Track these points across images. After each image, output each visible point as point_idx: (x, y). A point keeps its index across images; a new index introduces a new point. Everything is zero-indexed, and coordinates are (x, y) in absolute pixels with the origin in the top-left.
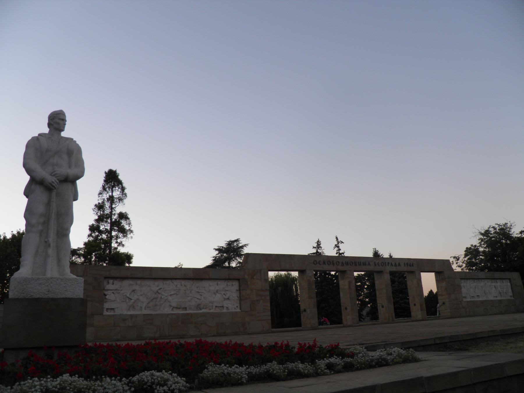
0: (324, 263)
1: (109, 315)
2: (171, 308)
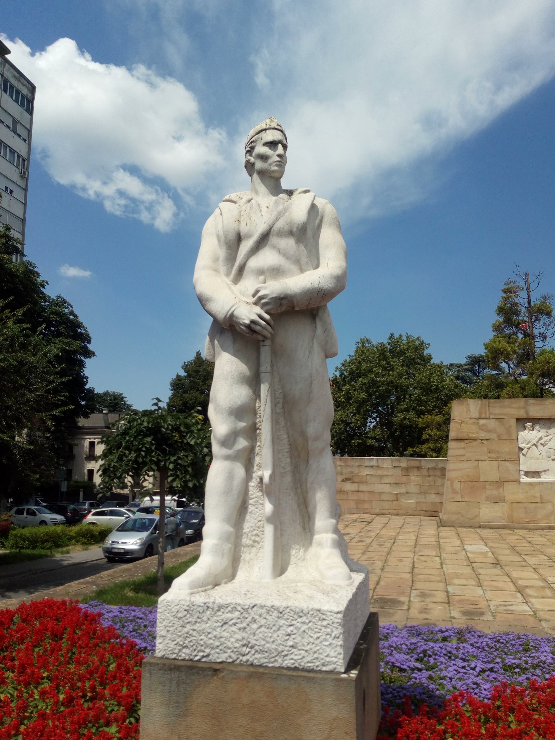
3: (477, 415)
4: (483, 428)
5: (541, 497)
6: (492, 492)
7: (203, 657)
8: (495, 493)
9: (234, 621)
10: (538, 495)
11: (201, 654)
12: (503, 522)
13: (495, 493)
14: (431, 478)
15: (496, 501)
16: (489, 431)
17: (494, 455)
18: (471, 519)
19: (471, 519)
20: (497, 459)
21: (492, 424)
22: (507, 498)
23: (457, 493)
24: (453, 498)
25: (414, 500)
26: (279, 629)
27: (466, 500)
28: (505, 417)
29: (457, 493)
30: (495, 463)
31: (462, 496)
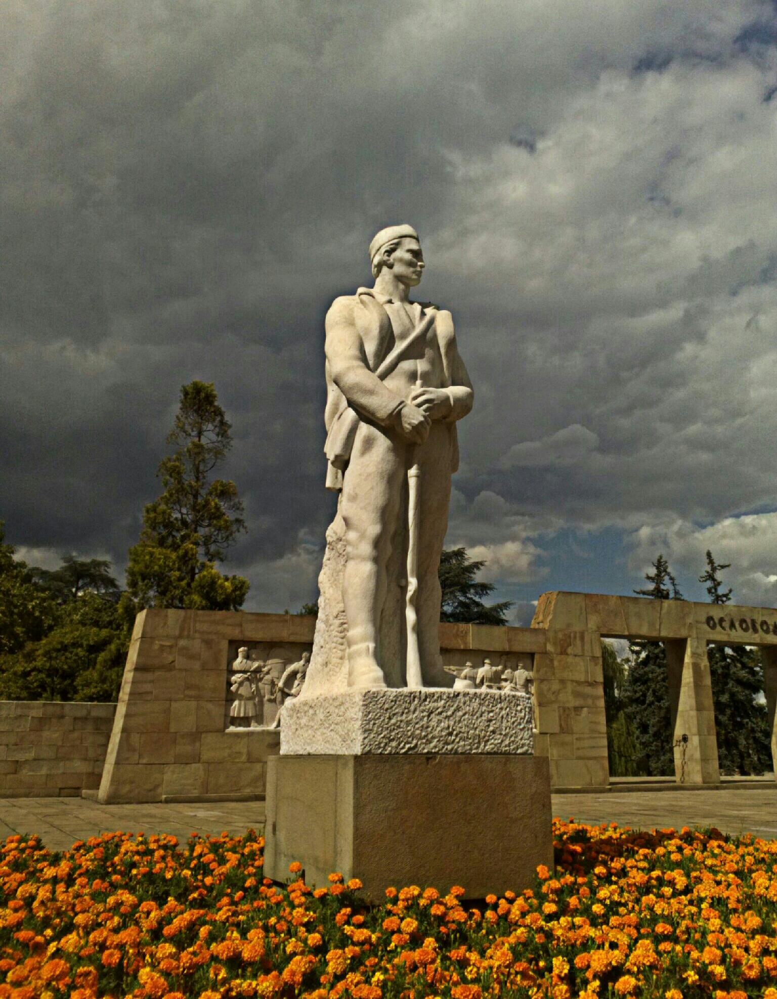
0: (732, 625)
1: (237, 735)
2: (397, 329)
3: (177, 633)
4: (184, 651)
5: (249, 754)
6: (184, 748)
7: (410, 749)
8: (189, 748)
9: (440, 710)
10: (245, 751)
11: (407, 746)
12: (195, 793)
13: (189, 748)
14: (76, 734)
15: (184, 761)
16: (192, 657)
17: (193, 693)
18: (150, 791)
19: (150, 791)
20: (198, 698)
21: (196, 645)
22: (205, 757)
23: (134, 750)
24: (127, 759)
25: (44, 771)
26: (481, 716)
27: (144, 761)
28: (214, 637)
29: (134, 750)
30: (193, 704)
31: (140, 756)
